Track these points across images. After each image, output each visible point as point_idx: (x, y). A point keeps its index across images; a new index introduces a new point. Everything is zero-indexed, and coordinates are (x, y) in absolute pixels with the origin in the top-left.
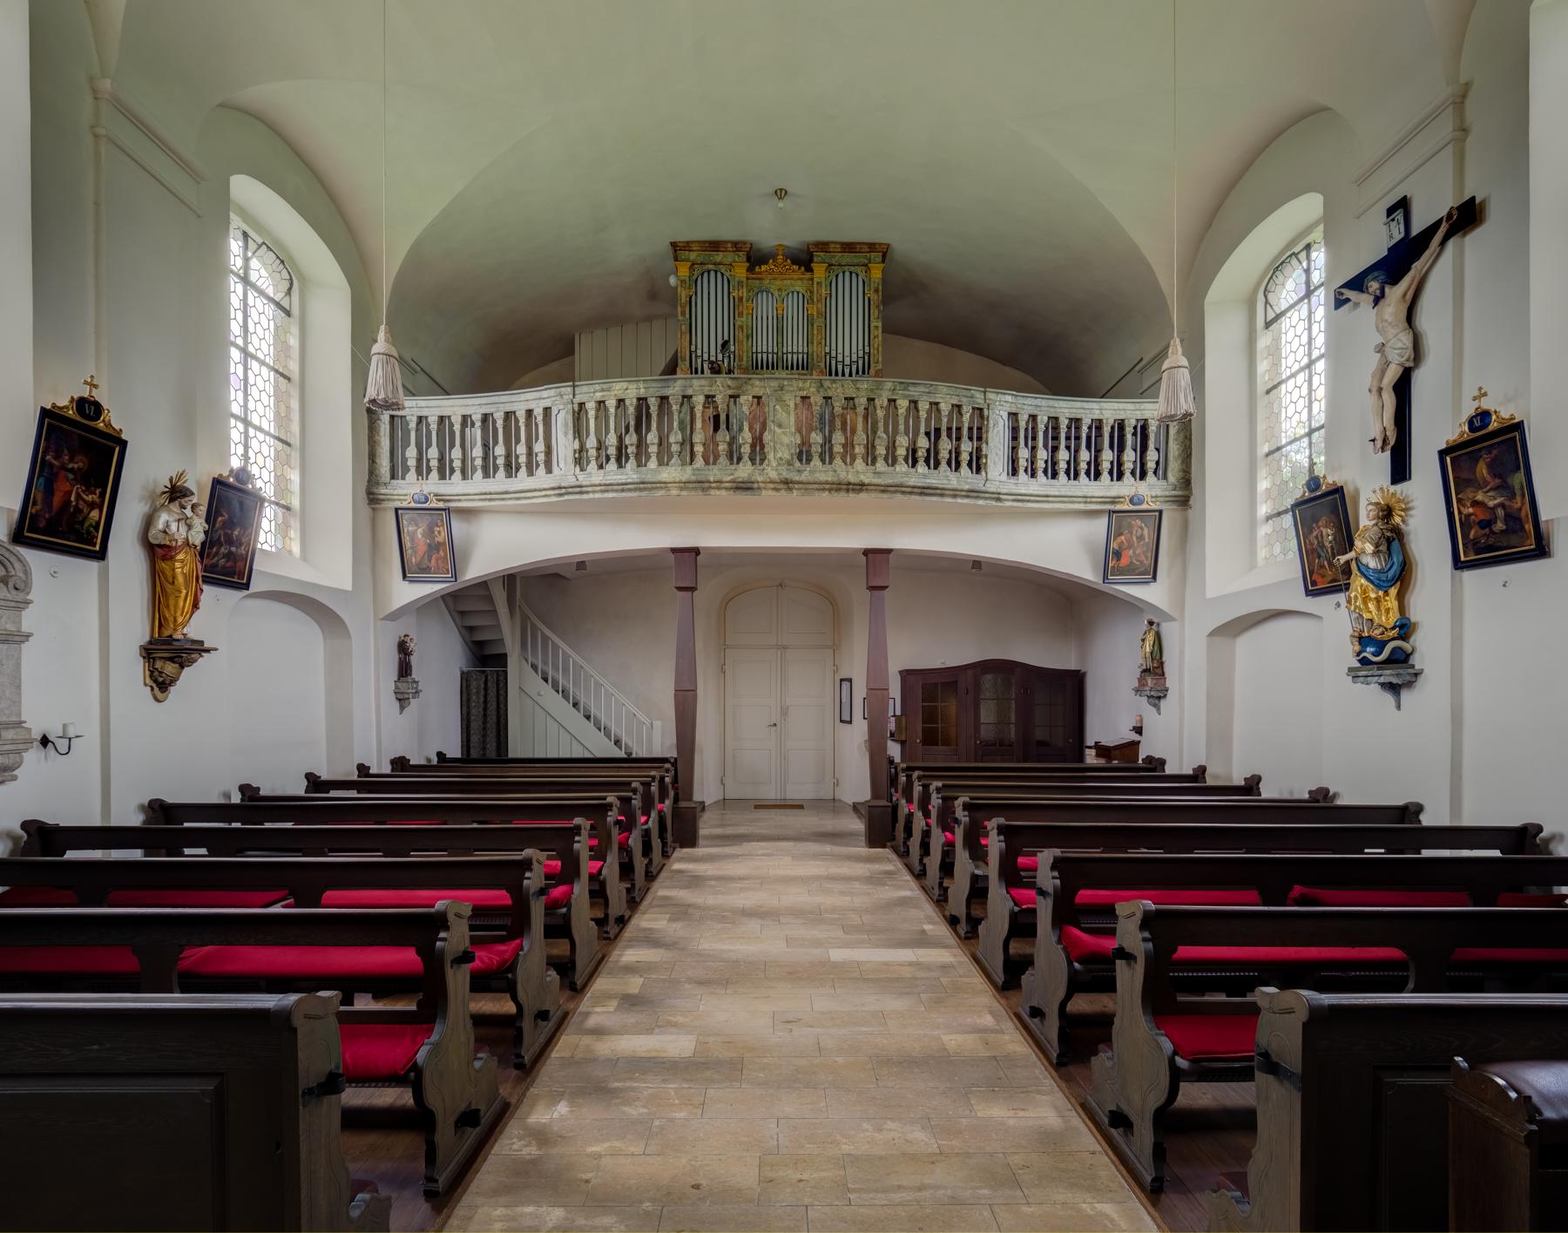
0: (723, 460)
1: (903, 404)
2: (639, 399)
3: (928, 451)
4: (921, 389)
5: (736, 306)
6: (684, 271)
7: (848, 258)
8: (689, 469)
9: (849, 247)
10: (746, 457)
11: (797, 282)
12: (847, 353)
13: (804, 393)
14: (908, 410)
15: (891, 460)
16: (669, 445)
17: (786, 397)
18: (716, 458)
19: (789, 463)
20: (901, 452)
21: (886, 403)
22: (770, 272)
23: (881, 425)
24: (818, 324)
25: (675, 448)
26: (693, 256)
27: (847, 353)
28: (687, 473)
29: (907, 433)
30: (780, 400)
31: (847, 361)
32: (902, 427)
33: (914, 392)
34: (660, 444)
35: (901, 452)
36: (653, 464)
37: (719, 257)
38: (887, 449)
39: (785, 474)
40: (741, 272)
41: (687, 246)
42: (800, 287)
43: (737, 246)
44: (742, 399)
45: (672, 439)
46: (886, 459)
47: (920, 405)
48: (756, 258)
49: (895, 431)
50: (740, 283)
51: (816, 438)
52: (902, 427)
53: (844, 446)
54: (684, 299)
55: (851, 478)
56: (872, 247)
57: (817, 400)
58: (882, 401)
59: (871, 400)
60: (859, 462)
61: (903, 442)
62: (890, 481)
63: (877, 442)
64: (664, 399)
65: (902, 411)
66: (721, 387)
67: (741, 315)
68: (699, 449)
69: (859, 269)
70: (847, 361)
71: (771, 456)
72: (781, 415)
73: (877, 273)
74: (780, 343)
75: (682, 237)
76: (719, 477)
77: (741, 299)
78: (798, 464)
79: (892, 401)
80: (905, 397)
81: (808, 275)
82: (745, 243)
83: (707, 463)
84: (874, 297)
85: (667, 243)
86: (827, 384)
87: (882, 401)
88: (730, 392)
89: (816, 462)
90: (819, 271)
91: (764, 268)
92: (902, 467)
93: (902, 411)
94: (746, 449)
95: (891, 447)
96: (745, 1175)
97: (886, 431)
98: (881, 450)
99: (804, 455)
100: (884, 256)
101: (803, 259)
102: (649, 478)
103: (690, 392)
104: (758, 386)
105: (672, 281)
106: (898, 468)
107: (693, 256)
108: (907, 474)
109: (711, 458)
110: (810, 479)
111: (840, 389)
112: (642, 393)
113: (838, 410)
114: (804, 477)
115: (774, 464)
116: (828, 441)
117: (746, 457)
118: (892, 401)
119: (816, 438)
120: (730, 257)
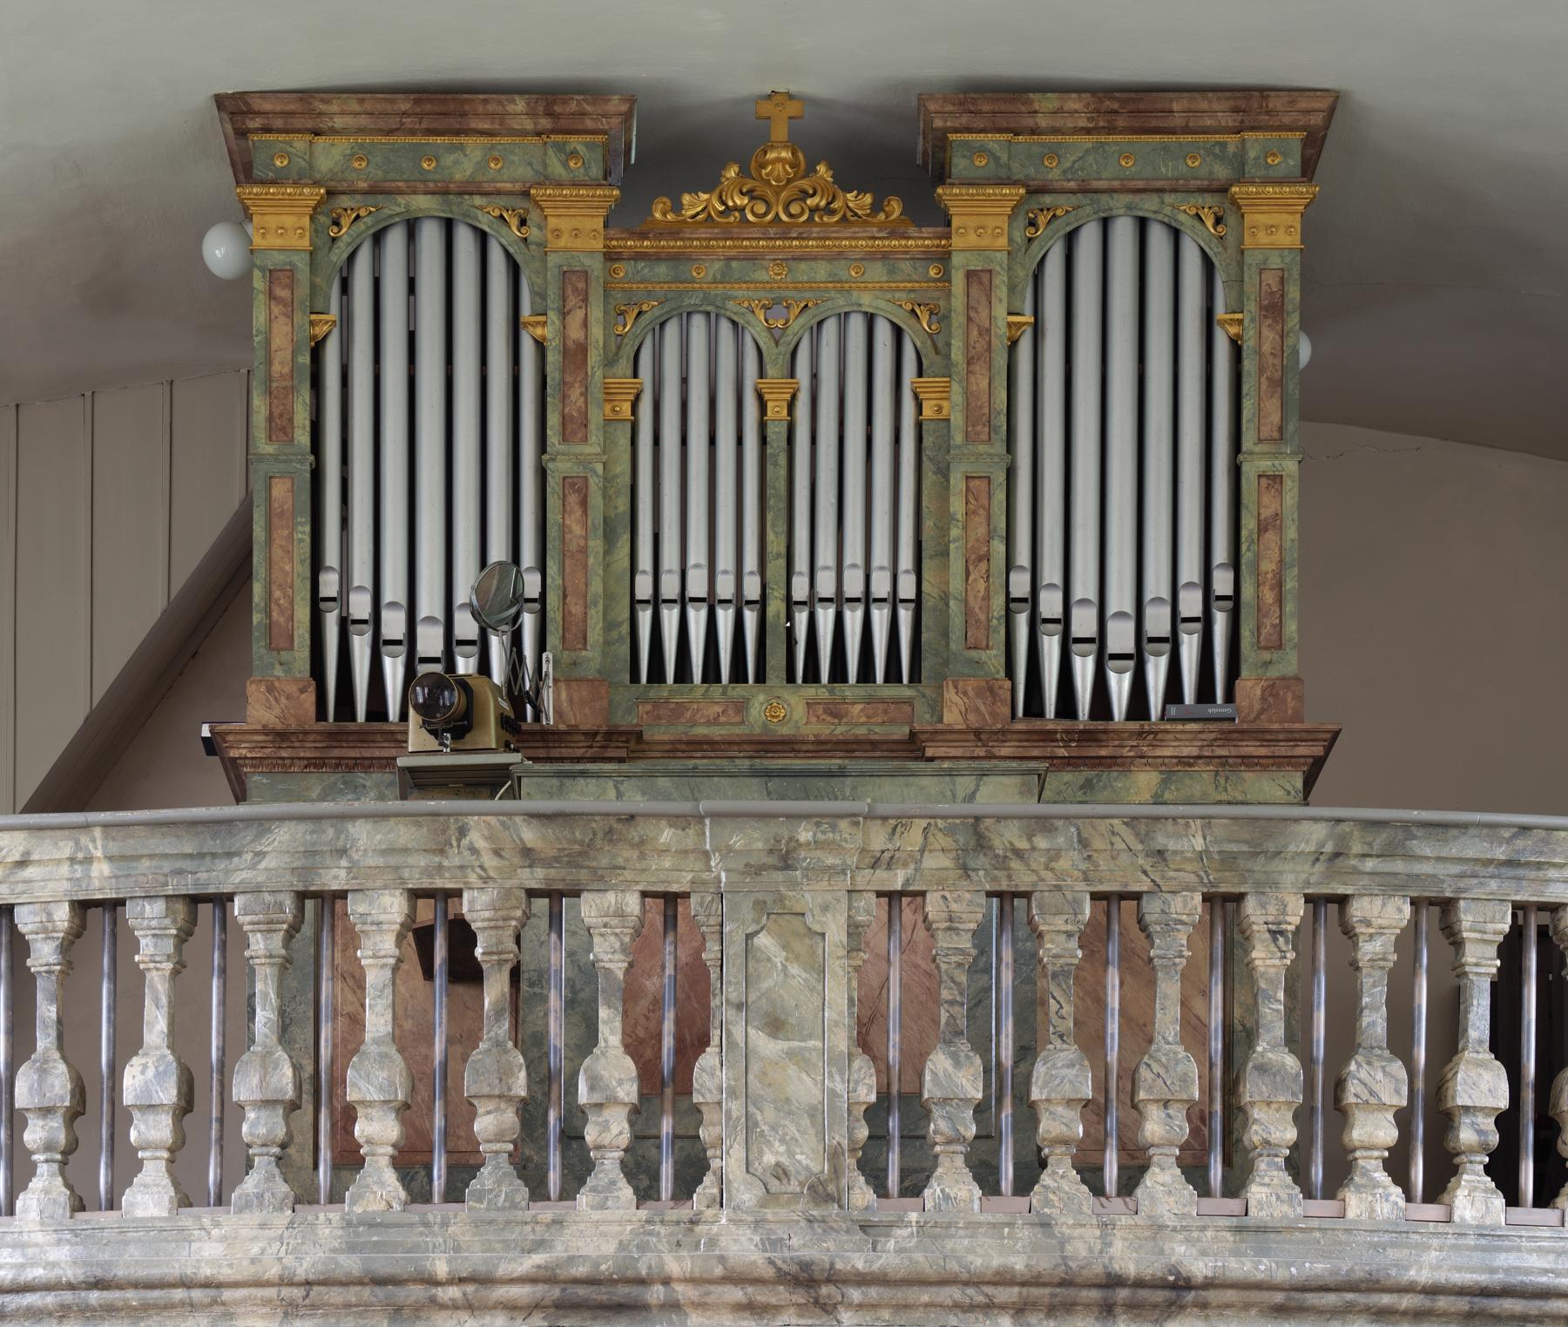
0: (495, 1180)
1: (1382, 917)
2: (82, 907)
3: (1507, 1122)
4: (1474, 848)
5: (550, 394)
6: (285, 227)
7: (1128, 156)
8: (327, 1222)
9: (1132, 106)
10: (609, 1166)
11: (865, 268)
12: (1120, 598)
13: (897, 880)
14: (1408, 941)
15: (1324, 1166)
16: (231, 1113)
17: (809, 897)
18: (464, 1169)
19: (822, 1193)
20: (1374, 1131)
21: (1296, 911)
22: (727, 224)
23: (1273, 1012)
24: (972, 465)
25: (257, 1126)
26: (329, 155)
27: (1120, 598)
28: (320, 1241)
29: (1400, 1043)
30: (773, 910)
31: (1121, 638)
32: (1375, 1020)
33: (1434, 862)
34: (186, 1105)
35: (1374, 1131)
36: (149, 1196)
37: (466, 159)
38: (1302, 1118)
39: (803, 1246)
40: (576, 229)
41: (305, 109)
42: (876, 290)
43: (557, 104)
44: (590, 908)
45: (245, 1088)
46: (1296, 1166)
47: (1467, 919)
48: (660, 154)
49: (1345, 1041)
50: (573, 280)
51: (953, 1077)
52: (1375, 1020)
53: (1094, 1110)
54: (286, 356)
55: (1127, 1258)
56: (1250, 103)
57: (958, 907)
58: (1277, 907)
59: (1224, 906)
60: (1164, 1184)
61: (1379, 1092)
62: (1317, 1268)
63: (1252, 1089)
64: (203, 908)
65: (1375, 949)
66: (485, 857)
67: (575, 428)
68: (378, 1130)
69: (1182, 210)
70: (1121, 638)
71: (730, 1161)
72: (780, 970)
73: (1274, 228)
74: (779, 558)
75: (280, 63)
76: (475, 1259)
77: (576, 355)
78: (862, 1194)
79: (1328, 906)
80: (1389, 885)
81: (922, 240)
82: (594, 91)
83: (418, 1193)
84: (1260, 339)
85: (201, 97)
86: (1008, 836)
87: (1277, 907)
88: (535, 877)
89: (952, 1183)
90: (980, 225)
91: (694, 203)
92: (1375, 1199)
93: (1375, 949)
94: (609, 1132)
95: (1326, 1109)
96: (61, 844)
97: (1297, 1040)
98: (1272, 1126)
99: (893, 1139)
100: (1314, 145)
101: (896, 159)
102: (131, 1261)
103: (334, 878)
104: (687, 841)
105: (220, 252)
106: (1355, 1203)
107: (329, 155)
108: (1399, 1231)
109: (435, 1164)
110: (923, 1262)
111: (1071, 851)
112: (100, 880)
113: (1060, 946)
114: (890, 1256)
115: (746, 1194)
116: (1010, 1091)
117: (609, 1166)
118: (1328, 906)
119: (953, 1077)
120: (514, 163)
